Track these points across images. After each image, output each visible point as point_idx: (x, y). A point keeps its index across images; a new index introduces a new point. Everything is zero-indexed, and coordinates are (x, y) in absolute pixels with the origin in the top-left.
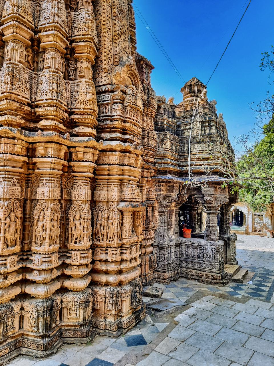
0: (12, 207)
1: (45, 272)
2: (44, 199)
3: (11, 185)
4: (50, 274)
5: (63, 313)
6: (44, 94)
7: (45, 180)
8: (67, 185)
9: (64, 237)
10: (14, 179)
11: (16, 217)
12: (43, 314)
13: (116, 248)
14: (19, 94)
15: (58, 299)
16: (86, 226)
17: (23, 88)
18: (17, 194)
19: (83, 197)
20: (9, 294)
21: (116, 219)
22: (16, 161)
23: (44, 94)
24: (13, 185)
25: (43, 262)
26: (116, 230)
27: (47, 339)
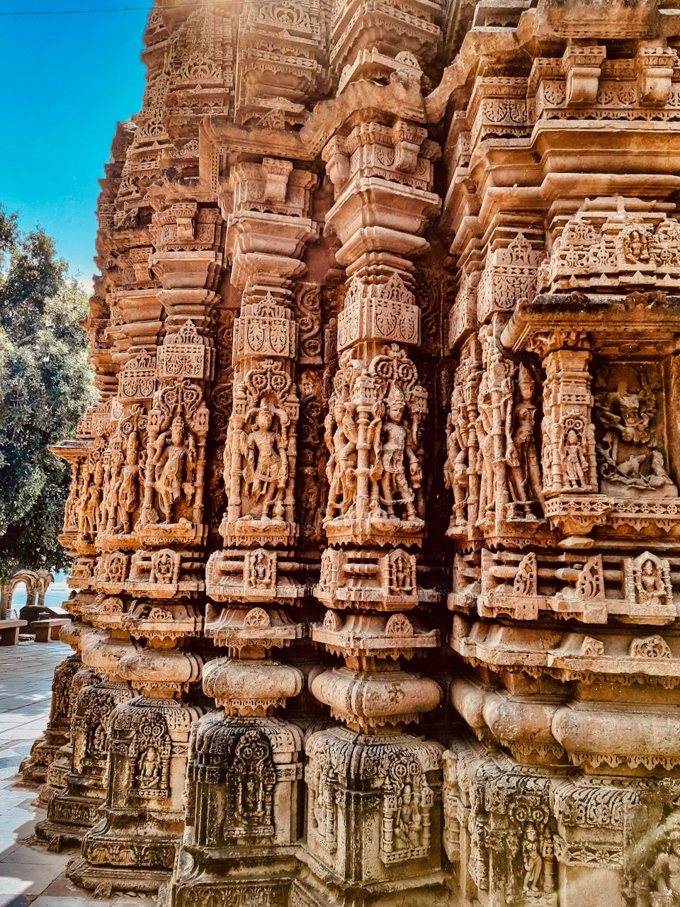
0: (177, 402)
1: (361, 619)
2: (274, 354)
3: (180, 340)
4: (379, 629)
5: (295, 806)
6: (196, 70)
7: (269, 294)
8: (303, 297)
9: (308, 487)
10: (189, 322)
11: (186, 431)
12: (345, 791)
13: (516, 550)
14: (194, 82)
15: (284, 739)
16: (361, 443)
17: (292, 8)
18: (194, 364)
19: (279, 347)
20: (153, 669)
21: (495, 397)
22: (187, 267)
23: (196, 70)
24: (184, 341)
25: (348, 575)
26: (497, 452)
27: (203, 875)
